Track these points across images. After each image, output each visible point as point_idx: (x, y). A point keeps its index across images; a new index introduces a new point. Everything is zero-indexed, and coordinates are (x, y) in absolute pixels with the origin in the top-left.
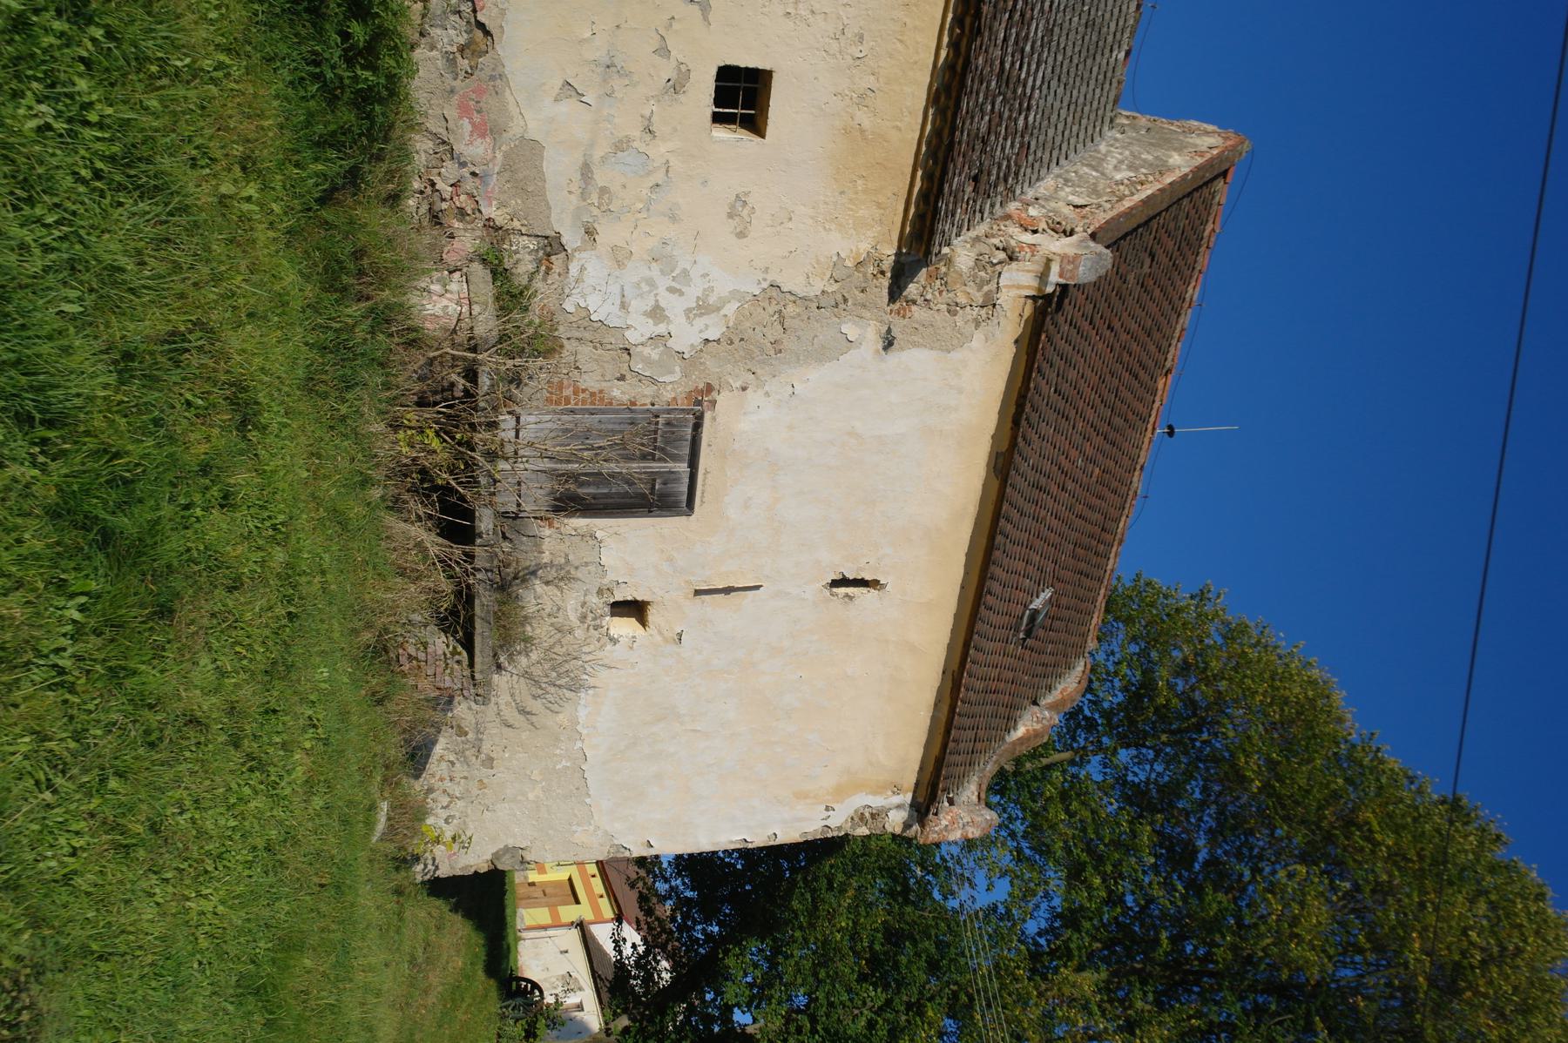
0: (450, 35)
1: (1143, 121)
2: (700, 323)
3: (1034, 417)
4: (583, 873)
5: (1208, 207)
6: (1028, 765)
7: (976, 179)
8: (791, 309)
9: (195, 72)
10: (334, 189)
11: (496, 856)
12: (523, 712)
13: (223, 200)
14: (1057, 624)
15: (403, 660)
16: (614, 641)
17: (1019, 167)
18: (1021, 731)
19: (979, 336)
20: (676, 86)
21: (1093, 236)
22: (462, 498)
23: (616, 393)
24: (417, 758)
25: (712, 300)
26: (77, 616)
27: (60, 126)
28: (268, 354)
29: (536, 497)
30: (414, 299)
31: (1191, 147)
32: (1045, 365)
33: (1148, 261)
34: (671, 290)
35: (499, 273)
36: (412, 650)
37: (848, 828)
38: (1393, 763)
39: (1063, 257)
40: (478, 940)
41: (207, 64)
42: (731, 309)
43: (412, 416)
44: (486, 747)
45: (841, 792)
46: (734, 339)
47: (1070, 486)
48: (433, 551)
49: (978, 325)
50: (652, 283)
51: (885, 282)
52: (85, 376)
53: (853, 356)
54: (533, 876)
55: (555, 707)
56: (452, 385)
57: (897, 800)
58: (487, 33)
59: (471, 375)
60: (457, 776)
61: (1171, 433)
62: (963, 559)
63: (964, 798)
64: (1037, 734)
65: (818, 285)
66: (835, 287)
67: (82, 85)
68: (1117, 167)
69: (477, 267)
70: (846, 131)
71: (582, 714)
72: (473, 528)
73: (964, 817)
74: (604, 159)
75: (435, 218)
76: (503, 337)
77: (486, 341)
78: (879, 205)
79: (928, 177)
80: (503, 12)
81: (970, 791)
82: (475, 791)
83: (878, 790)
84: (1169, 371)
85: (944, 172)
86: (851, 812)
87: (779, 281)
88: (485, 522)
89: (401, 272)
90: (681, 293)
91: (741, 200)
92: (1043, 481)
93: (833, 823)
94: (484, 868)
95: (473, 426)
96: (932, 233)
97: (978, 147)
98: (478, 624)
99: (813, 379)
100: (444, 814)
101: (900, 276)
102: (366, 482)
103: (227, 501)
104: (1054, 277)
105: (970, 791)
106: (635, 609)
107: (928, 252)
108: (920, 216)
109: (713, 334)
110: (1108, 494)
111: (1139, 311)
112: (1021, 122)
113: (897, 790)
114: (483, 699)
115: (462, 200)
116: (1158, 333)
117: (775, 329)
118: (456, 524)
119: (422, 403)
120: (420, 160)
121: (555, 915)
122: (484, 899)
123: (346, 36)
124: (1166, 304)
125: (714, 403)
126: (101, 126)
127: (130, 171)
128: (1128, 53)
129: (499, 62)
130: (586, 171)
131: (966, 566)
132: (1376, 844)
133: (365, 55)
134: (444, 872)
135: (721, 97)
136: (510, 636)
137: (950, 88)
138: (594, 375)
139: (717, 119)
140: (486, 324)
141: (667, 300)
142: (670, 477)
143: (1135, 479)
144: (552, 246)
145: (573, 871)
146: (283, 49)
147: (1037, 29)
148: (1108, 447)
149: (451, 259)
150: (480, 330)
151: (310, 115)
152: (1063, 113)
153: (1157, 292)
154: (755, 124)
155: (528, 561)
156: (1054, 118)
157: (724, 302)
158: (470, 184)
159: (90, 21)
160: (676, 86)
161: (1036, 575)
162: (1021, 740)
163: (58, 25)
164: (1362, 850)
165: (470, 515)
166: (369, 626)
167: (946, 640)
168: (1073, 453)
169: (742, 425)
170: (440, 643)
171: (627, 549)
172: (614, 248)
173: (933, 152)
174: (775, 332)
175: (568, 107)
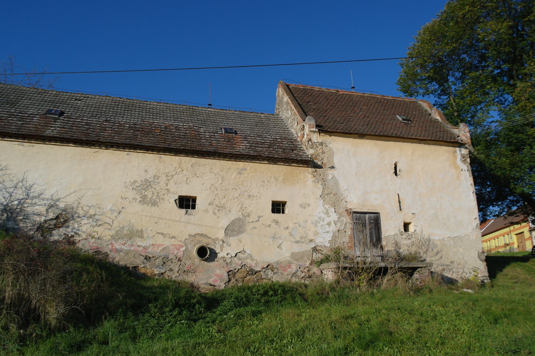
0: (270, 273)
1: (277, 106)
2: (331, 214)
3: (349, 129)
4: (513, 231)
5: (296, 89)
6: (455, 108)
7: (293, 150)
8: (326, 192)
9: (281, 323)
10: (304, 299)
11: (481, 260)
12: (437, 253)
13: (306, 319)
14: (407, 112)
15: (421, 285)
16: (415, 231)
17: (290, 139)
18: (438, 118)
19: (330, 146)
20: (277, 222)
21: (304, 121)
22: (376, 270)
23: (349, 233)
24: (451, 282)
25: (325, 211)
26: (387, 348)
27: (292, 345)
28: (337, 312)
29: (376, 252)
30: (328, 282)
31: (283, 96)
32: (336, 128)
33: (310, 103)
34: (323, 221)
35: (321, 262)
36: (418, 283)
37: (468, 164)
38: (445, 8)
39: (309, 128)
40: (513, 264)
41: (279, 322)
42: (327, 206)
43: (357, 282)
44: (448, 263)
45: (457, 167)
46: (334, 205)
47: (368, 115)
48: (390, 277)
49: (327, 146)
50: (322, 226)
51: (318, 170)
52: (339, 343)
53: (337, 176)
54: (516, 246)
55: (436, 245)
56: (348, 273)
57: (458, 152)
58: (269, 265)
59: (345, 268)
60: (457, 271)
61: (354, 88)
62: (388, 142)
63: (457, 133)
64: (439, 113)
65: (320, 186)
66: (320, 182)
67: (285, 341)
68: (287, 112)
69: (321, 267)
70: (284, 182)
71: (436, 238)
72: (384, 268)
73: (463, 132)
74: (294, 238)
75: (310, 277)
76: (336, 261)
77: (337, 265)
78: (300, 173)
79: (293, 162)
80: (264, 262)
81: (456, 131)
82: (461, 266)
83: (455, 157)
84: (338, 91)
85: (292, 159)
86: (462, 164)
87: (319, 195)
88: (382, 265)
89: (322, 284)
90: (324, 219)
91: (301, 206)
92: (366, 123)
93: (466, 168)
94: (485, 263)
95: (358, 268)
96: (306, 160)
97: (285, 151)
98: (410, 266)
99: (343, 185)
100: (468, 275)
101: (317, 166)
102: (373, 294)
103: (368, 321)
104: (314, 129)
105: (456, 131)
106: (406, 226)
107: (310, 161)
108: (302, 163)
109: (333, 210)
110: (370, 103)
111: (322, 103)
112: (279, 140)
113: (455, 152)
114: (431, 265)
115: (306, 270)
116: (327, 96)
117: (331, 196)
118: (383, 271)
119: (353, 280)
120: (297, 280)
121: (528, 239)
122: (496, 263)
123: (272, 296)
124: (320, 96)
125: (350, 209)
126: (292, 339)
127: (300, 335)
128: (262, 114)
129: (275, 263)
130: (297, 242)
131: (389, 141)
132: (469, 11)
133: (275, 291)
134: (487, 274)
135: (278, 211)
136: (414, 257)
137: (273, 160)
138: (345, 239)
139: (283, 213)
140: (333, 265)
141: (326, 222)
142: (370, 219)
143: (366, 95)
144: (315, 249)
145: (513, 234)
146: (275, 309)
147: (258, 140)
148: (357, 106)
149: (319, 273)
150: (334, 266)
151: (288, 303)
152: (276, 129)
153: (317, 99)
154: (284, 204)
155: (394, 254)
156: (278, 131)
157: (325, 208)
158: (302, 269)
159: (273, 340)
160: (277, 222)
161: (392, 121)
162: (441, 118)
163: (275, 344)
164: (471, 15)
165: (380, 268)
166: (409, 293)
167: (410, 144)
168: (359, 115)
169: (356, 201)
170: (416, 275)
171: (390, 229)
172: (314, 235)
173: (287, 162)
174: (332, 195)
175: (283, 246)
